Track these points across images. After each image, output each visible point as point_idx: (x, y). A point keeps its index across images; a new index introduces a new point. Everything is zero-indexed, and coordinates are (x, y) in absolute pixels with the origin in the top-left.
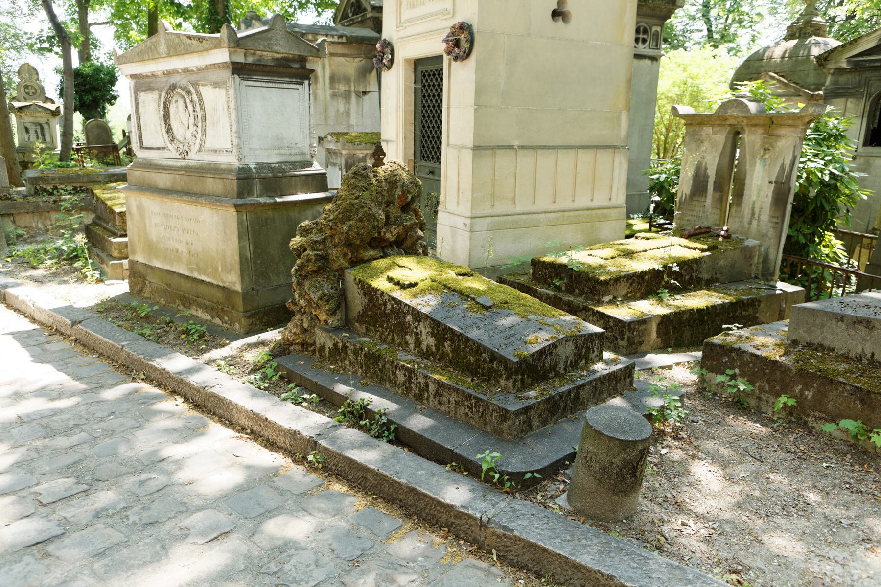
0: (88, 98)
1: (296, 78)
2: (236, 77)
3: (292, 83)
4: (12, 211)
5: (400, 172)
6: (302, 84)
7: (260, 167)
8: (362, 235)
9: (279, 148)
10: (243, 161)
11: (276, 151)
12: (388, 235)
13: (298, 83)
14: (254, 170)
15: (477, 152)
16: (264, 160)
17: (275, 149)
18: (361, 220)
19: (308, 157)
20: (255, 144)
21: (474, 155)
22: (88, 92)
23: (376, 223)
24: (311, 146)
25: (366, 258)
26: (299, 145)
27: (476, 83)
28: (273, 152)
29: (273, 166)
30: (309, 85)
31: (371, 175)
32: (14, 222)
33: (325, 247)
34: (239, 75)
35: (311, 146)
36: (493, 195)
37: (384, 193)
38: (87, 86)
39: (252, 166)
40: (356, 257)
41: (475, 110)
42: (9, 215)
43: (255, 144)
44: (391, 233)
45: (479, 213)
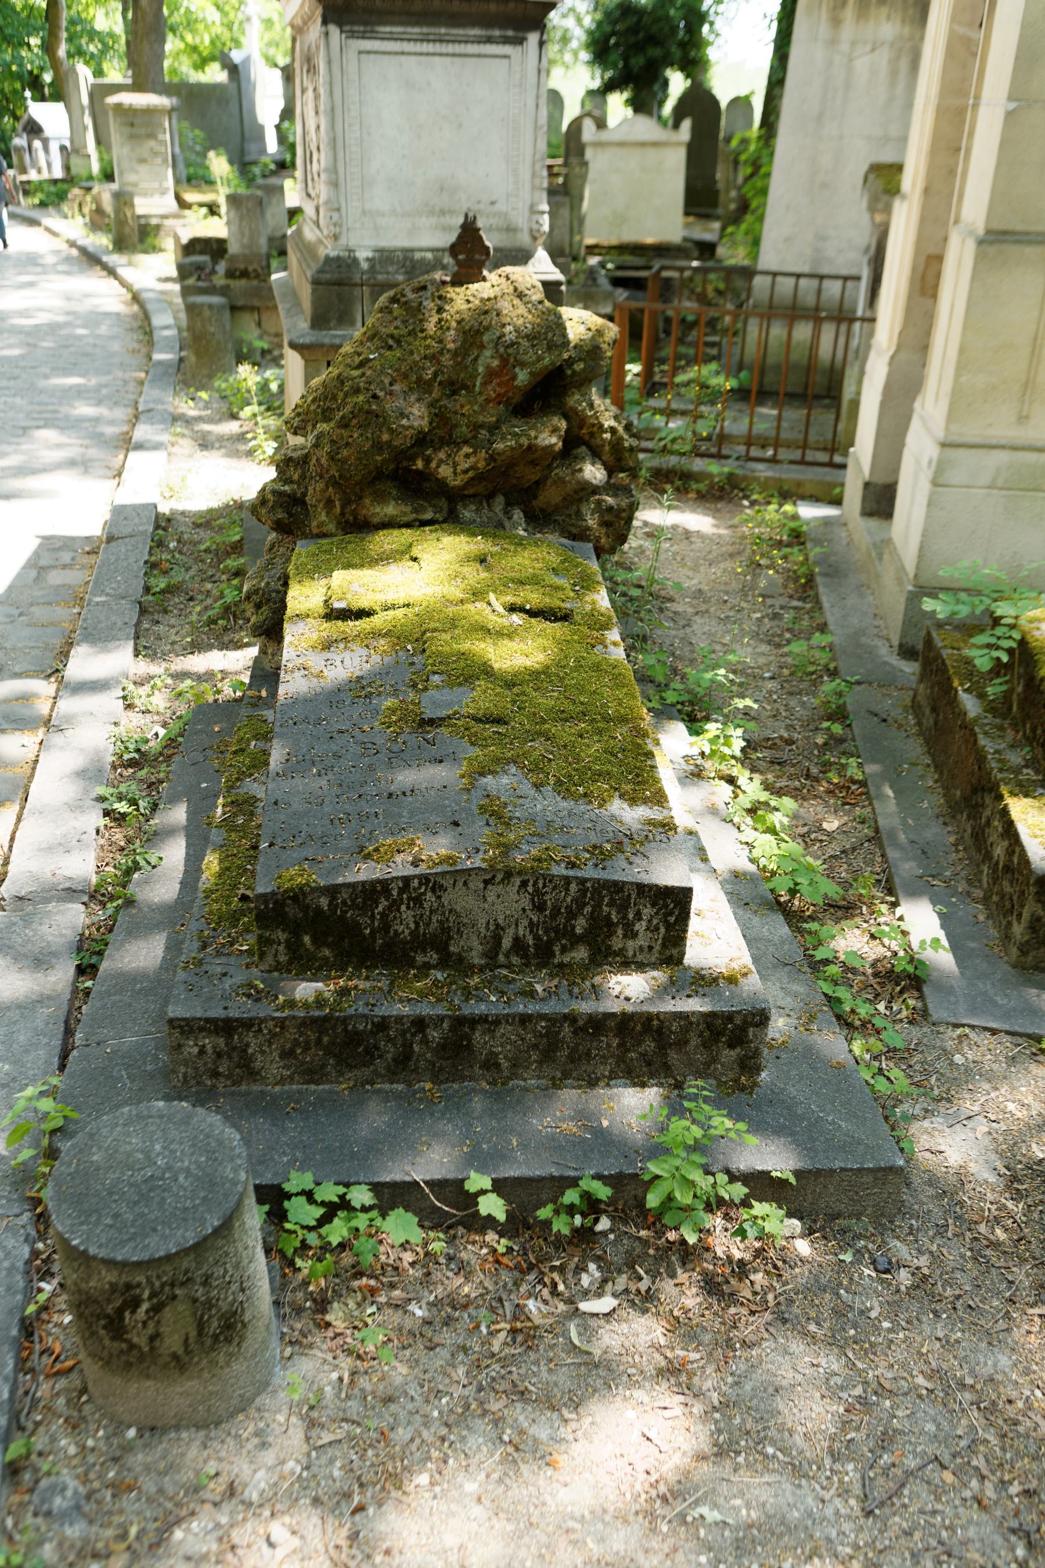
0: (638, 62)
1: (503, 26)
2: (334, 30)
3: (489, 40)
4: (256, 302)
5: (505, 306)
6: (520, 41)
7: (384, 257)
8: (344, 461)
9: (443, 213)
10: (343, 241)
11: (433, 220)
12: (445, 471)
13: (506, 41)
14: (365, 266)
15: (992, 250)
16: (397, 239)
17: (431, 213)
18: (344, 424)
19: (524, 239)
20: (380, 199)
21: (980, 258)
22: (638, 48)
23: (385, 437)
24: (533, 211)
25: (376, 520)
26: (501, 207)
27: (1024, 27)
28: (426, 222)
29: (418, 256)
30: (542, 44)
31: (429, 305)
32: (259, 324)
33: (303, 477)
34: (340, 25)
35: (533, 211)
36: (1028, 386)
37: (446, 360)
38: (641, 35)
39: (362, 255)
40: (354, 513)
41: (1009, 115)
42: (252, 309)
43: (380, 199)
44: (455, 465)
45: (972, 432)
